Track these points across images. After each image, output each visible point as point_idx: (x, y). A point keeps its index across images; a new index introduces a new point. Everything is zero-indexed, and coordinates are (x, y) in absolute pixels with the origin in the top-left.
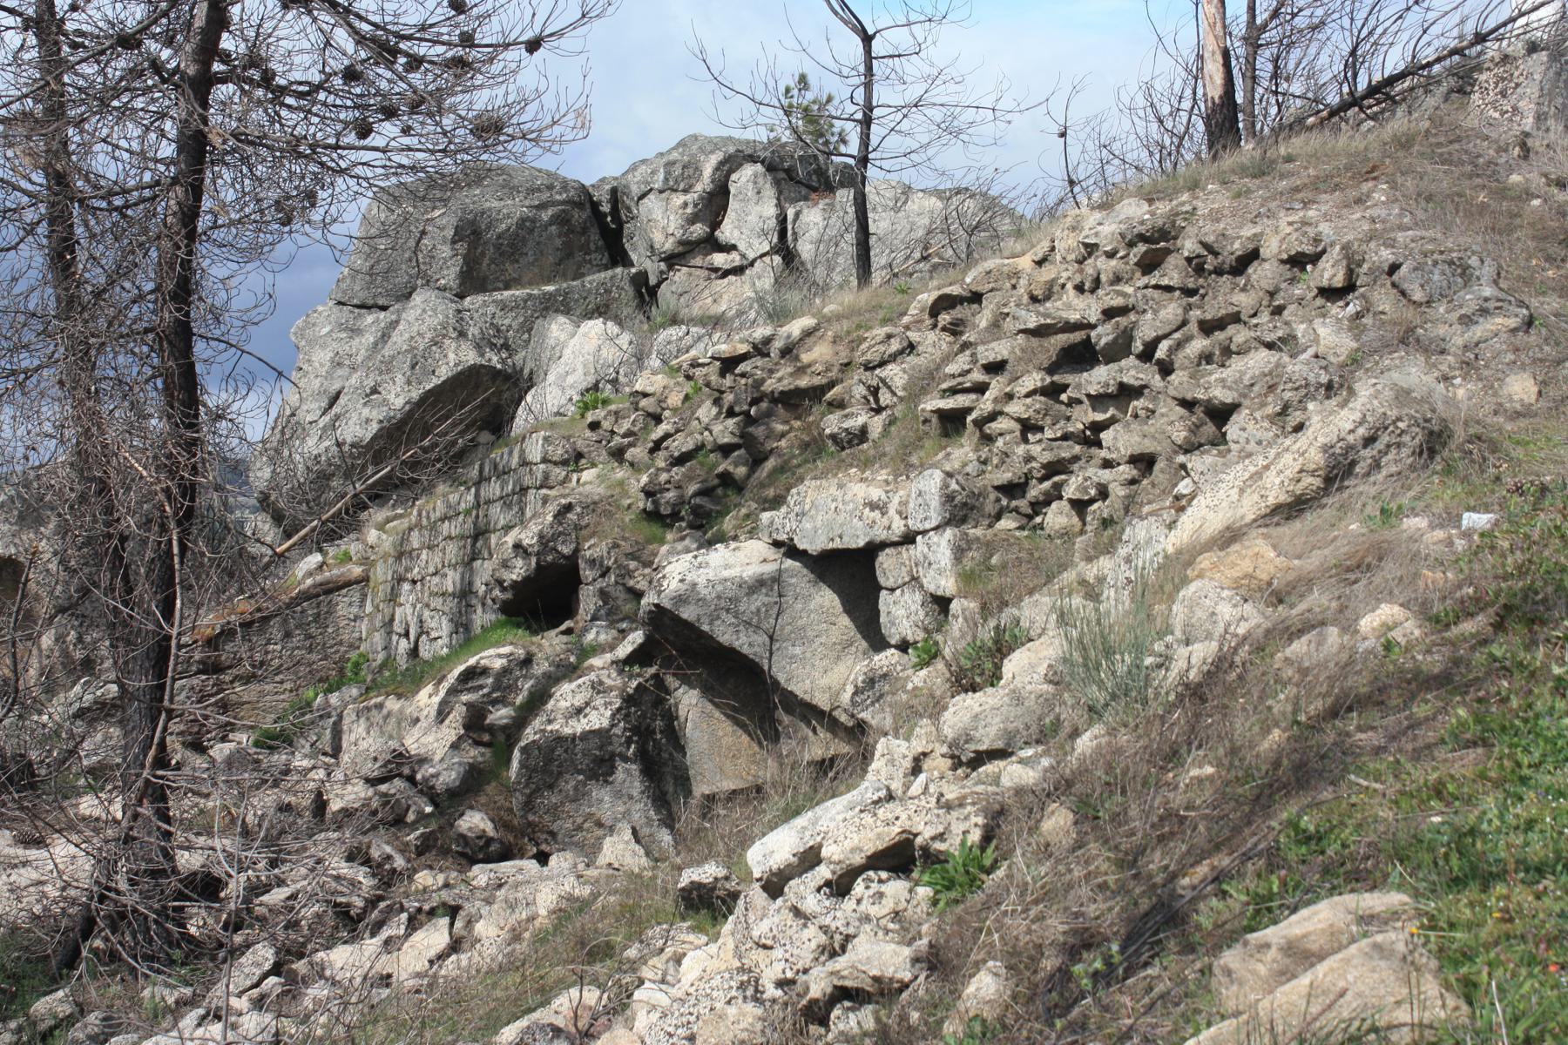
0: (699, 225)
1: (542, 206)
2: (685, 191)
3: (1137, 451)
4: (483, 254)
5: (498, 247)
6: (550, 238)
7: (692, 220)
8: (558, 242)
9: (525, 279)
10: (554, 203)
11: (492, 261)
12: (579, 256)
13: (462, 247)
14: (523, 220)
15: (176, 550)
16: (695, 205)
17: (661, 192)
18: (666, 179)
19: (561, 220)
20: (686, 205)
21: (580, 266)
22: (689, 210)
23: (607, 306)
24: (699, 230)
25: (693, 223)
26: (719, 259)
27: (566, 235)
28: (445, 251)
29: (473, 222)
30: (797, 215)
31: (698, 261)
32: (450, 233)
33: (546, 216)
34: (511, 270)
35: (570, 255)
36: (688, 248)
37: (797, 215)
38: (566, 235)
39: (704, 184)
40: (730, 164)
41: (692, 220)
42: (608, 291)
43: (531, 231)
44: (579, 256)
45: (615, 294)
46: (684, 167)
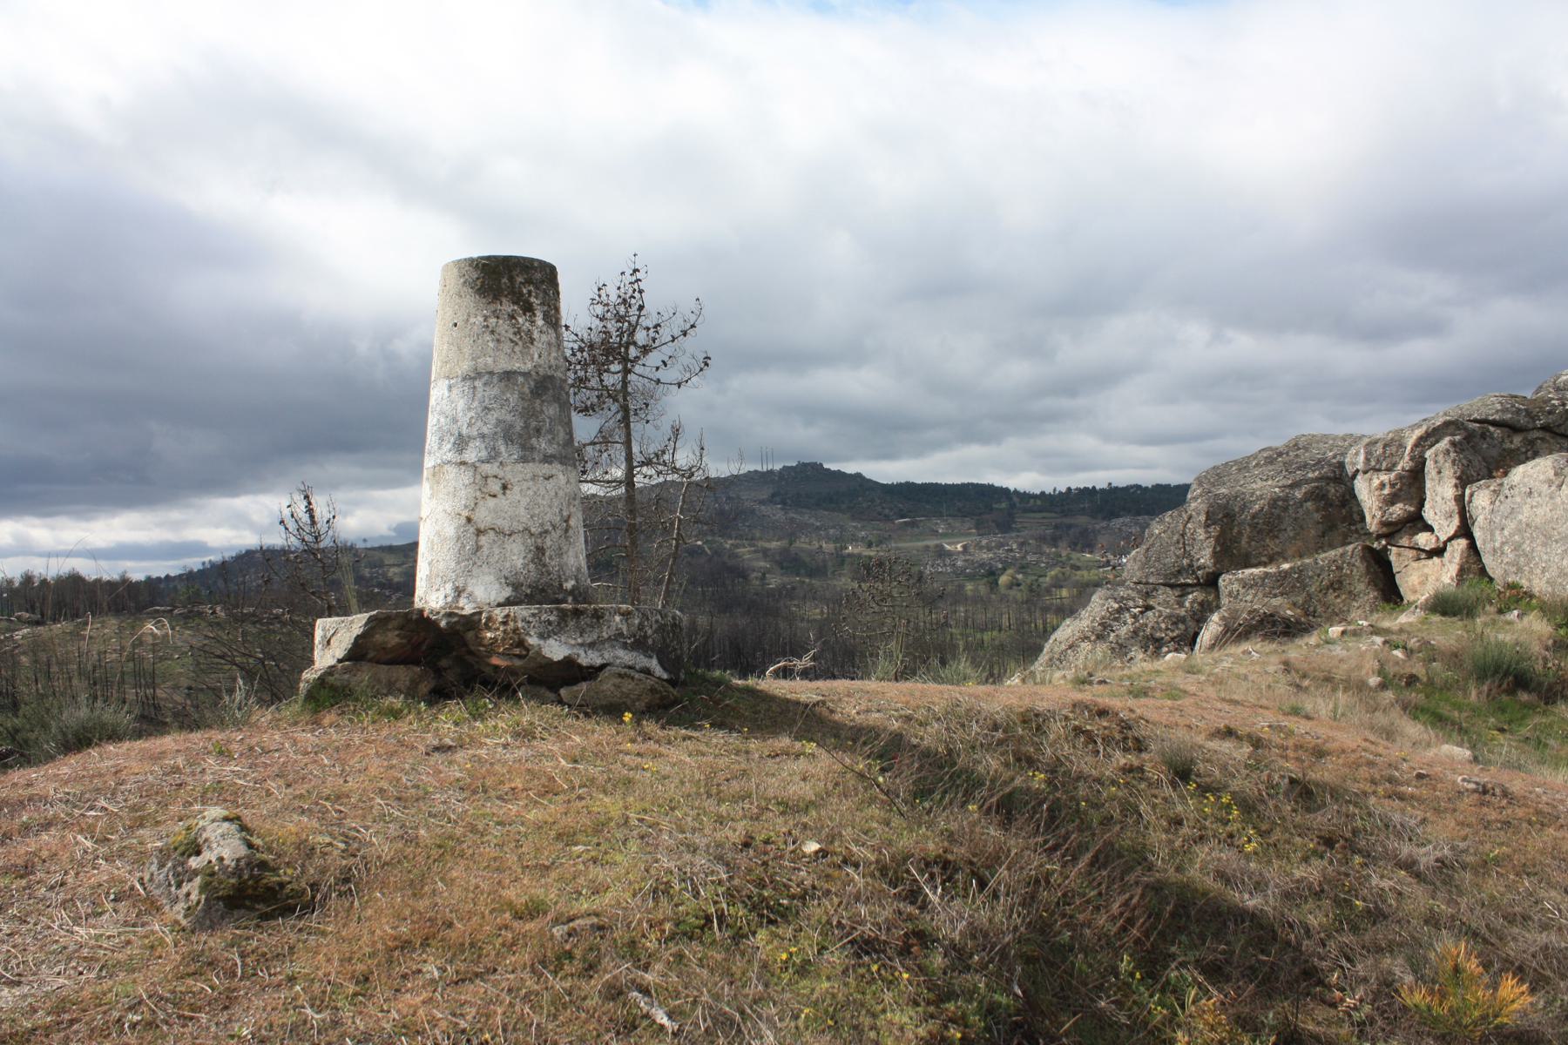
0: (1400, 505)
1: (1295, 485)
2: (1389, 470)
3: (284, 931)
4: (1240, 533)
5: (1254, 526)
6: (1308, 512)
7: (1391, 500)
8: (1317, 516)
9: (1290, 553)
10: (1308, 481)
11: (1251, 539)
12: (1343, 528)
13: (1215, 530)
14: (1274, 502)
15: (1088, 857)
16: (1392, 485)
17: (1365, 472)
18: (1367, 460)
19: (1317, 496)
20: (1382, 485)
21: (1345, 536)
22: (1386, 491)
23: (1340, 582)
24: (1398, 510)
25: (1393, 504)
26: (1423, 539)
27: (1325, 509)
28: (1201, 534)
29: (1225, 507)
30: (1472, 495)
31: (1404, 541)
32: (1203, 518)
33: (1298, 494)
34: (1273, 546)
35: (1332, 527)
36: (1392, 529)
37: (1472, 495)
38: (1325, 509)
39: (1405, 463)
40: (1431, 437)
41: (1391, 500)
42: (1340, 568)
43: (1285, 509)
44: (1343, 528)
45: (1346, 571)
46: (1385, 446)
